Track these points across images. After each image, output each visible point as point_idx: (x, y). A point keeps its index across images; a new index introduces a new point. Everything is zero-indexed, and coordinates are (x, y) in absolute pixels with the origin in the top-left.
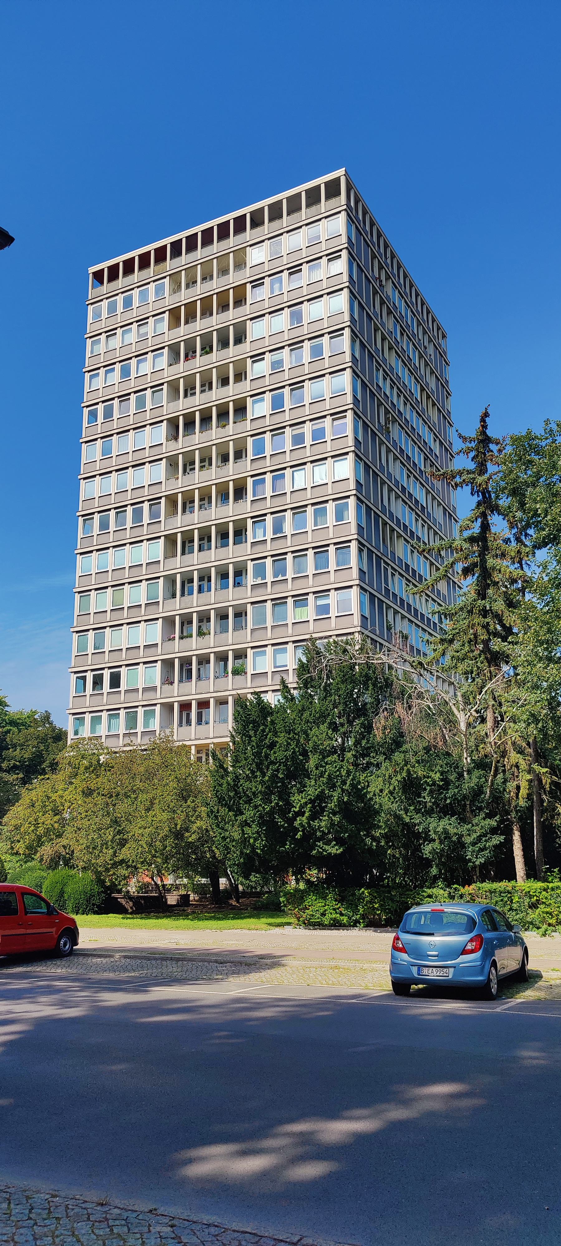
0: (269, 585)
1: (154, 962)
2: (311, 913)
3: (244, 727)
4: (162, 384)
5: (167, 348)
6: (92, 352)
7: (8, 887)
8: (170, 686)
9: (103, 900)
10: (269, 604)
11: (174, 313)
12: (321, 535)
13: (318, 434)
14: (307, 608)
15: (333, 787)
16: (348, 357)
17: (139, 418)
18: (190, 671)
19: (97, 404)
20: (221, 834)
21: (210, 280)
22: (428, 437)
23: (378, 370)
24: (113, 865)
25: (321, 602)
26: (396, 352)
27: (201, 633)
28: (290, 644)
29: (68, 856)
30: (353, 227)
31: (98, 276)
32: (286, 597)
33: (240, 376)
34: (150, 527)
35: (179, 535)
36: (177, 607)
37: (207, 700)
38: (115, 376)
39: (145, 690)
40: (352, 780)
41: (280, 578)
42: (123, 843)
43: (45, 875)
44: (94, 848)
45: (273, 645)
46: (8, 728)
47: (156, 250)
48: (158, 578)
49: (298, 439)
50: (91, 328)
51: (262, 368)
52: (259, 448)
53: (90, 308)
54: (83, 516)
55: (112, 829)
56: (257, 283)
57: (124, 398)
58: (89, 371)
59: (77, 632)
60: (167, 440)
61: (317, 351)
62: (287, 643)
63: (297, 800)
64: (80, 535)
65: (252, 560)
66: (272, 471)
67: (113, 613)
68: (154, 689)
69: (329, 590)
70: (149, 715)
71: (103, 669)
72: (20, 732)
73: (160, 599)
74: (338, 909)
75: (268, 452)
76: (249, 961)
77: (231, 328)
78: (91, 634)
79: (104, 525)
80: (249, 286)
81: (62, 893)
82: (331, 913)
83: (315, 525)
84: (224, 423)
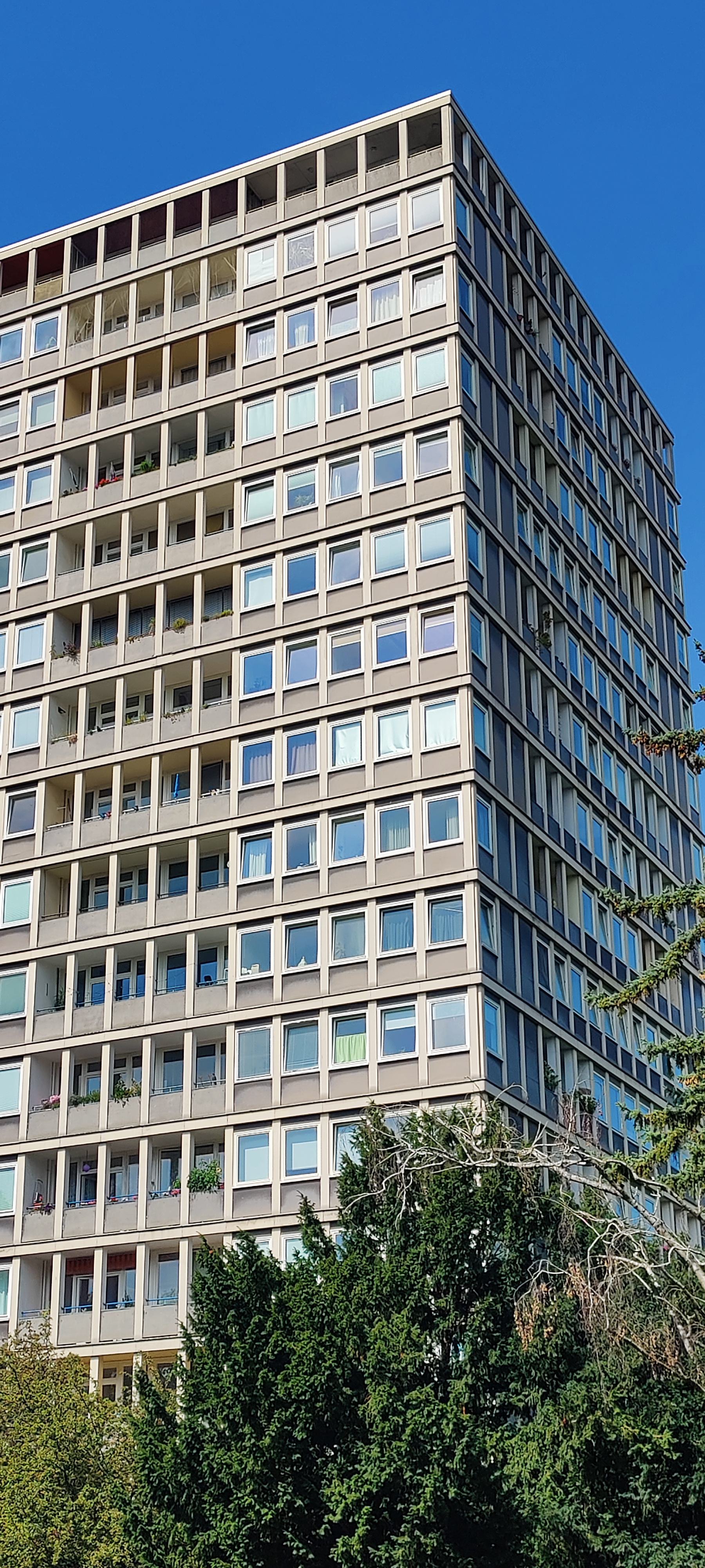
3: (216, 1318)
4: (47, 534)
8: (45, 1216)
13: (392, 648)
15: (421, 1462)
21: (157, 315)
22: (634, 657)
25: (395, 1023)
27: (119, 1093)
30: (469, 210)
40: (468, 1446)
41: (302, 967)
48: (25, 963)
49: (346, 658)
51: (270, 502)
52: (260, 675)
56: (260, 323)
60: (54, 657)
62: (316, 1117)
63: (339, 1494)
65: (240, 925)
69: (413, 996)
73: (29, 1012)
77: (201, 416)
80: (241, 329)
83: (384, 848)
84: (182, 620)
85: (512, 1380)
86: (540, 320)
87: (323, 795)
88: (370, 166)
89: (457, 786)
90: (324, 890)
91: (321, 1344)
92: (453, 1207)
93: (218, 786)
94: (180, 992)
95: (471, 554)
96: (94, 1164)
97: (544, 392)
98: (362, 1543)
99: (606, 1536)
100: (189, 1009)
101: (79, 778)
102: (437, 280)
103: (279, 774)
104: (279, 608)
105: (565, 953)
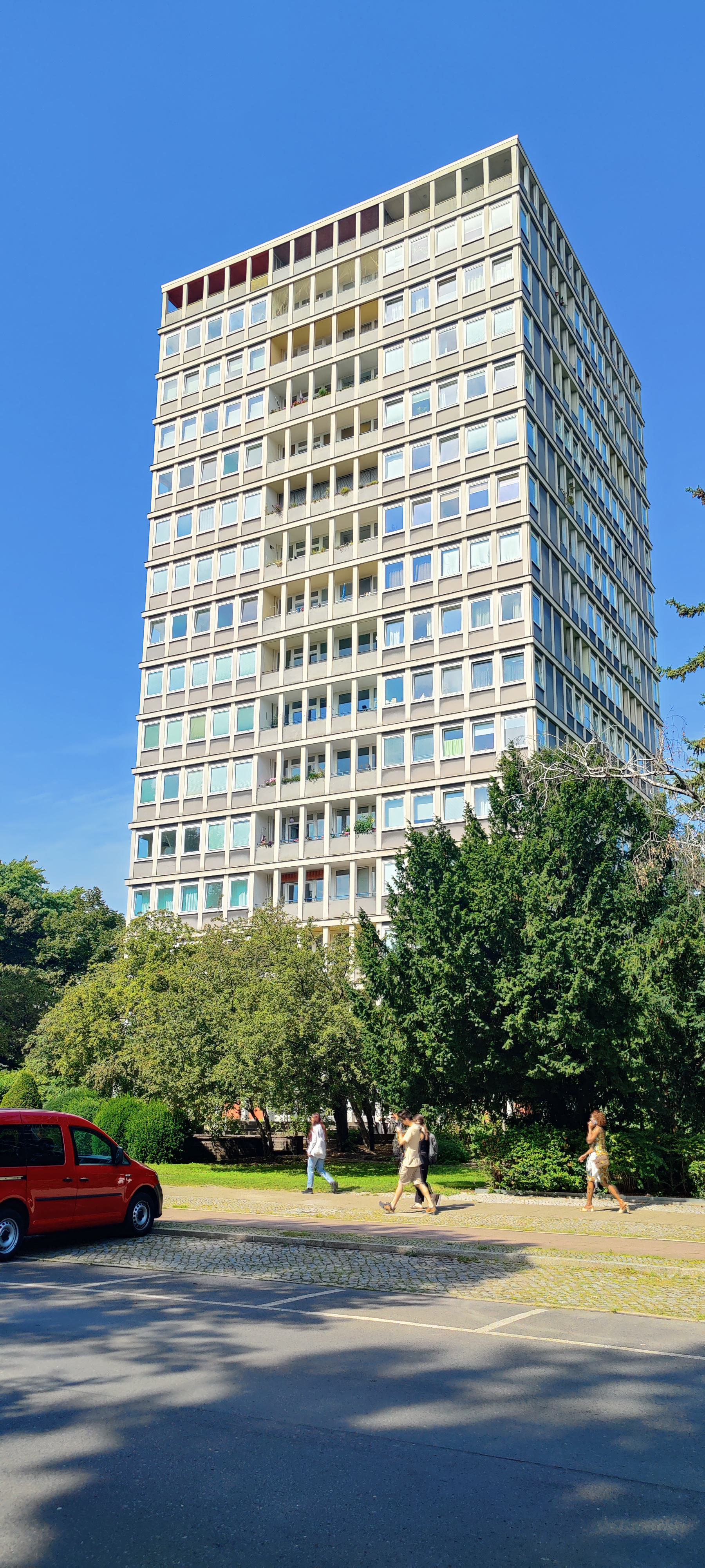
0: (408, 708)
1: (294, 1249)
2: (522, 1169)
3: (421, 872)
4: (261, 438)
6: (165, 398)
7: (46, 1116)
8: (268, 848)
9: (181, 1142)
10: (408, 735)
11: (278, 343)
12: (482, 639)
13: (479, 501)
14: (458, 739)
15: (568, 965)
16: (520, 394)
17: (228, 483)
18: (295, 830)
19: (172, 466)
20: (376, 1042)
21: (327, 296)
22: (620, 518)
23: (558, 418)
24: (200, 1089)
25: (481, 732)
26: (581, 397)
27: (311, 776)
28: (438, 790)
29: (129, 1078)
30: (528, 217)
31: (175, 297)
32: (432, 725)
33: (367, 426)
34: (242, 631)
35: (282, 642)
36: (278, 739)
37: (320, 867)
38: (197, 429)
39: (234, 853)
40: (604, 954)
41: (423, 698)
42: (214, 1060)
43: (97, 1104)
44: (172, 1064)
45: (413, 791)
46: (45, 909)
47: (254, 258)
48: (253, 700)
49: (450, 509)
50: (163, 366)
51: (401, 411)
52: (395, 521)
53: (161, 383)
54: (150, 617)
55: (199, 1036)
56: (393, 297)
57: (208, 457)
58: (161, 423)
59: (141, 774)
60: (267, 514)
61: (477, 388)
62: (432, 788)
63: (506, 988)
64: (147, 643)
65: (384, 674)
66: (412, 553)
67: (190, 748)
68: (246, 852)
69: (493, 715)
70: (238, 888)
71: (176, 824)
72: (60, 915)
73: (256, 729)
74: (566, 1163)
75: (408, 526)
76: (465, 1252)
77: (357, 359)
78: (160, 777)
79: (179, 630)
80: (382, 302)
81: (121, 1130)
82: (555, 1171)
83: (474, 626)
84: (346, 488)
85: (612, 919)
86: (568, 298)
87: (436, 593)
88: (464, 190)
89: (520, 585)
90: (436, 652)
91: (496, 889)
92: (572, 806)
93: (369, 590)
94: (348, 716)
96: (297, 818)
97: (570, 345)
98: (524, 1018)
99: (688, 1017)
100: (354, 725)
101: (284, 588)
102: (508, 263)
103: (408, 580)
104: (407, 478)
105: (581, 692)
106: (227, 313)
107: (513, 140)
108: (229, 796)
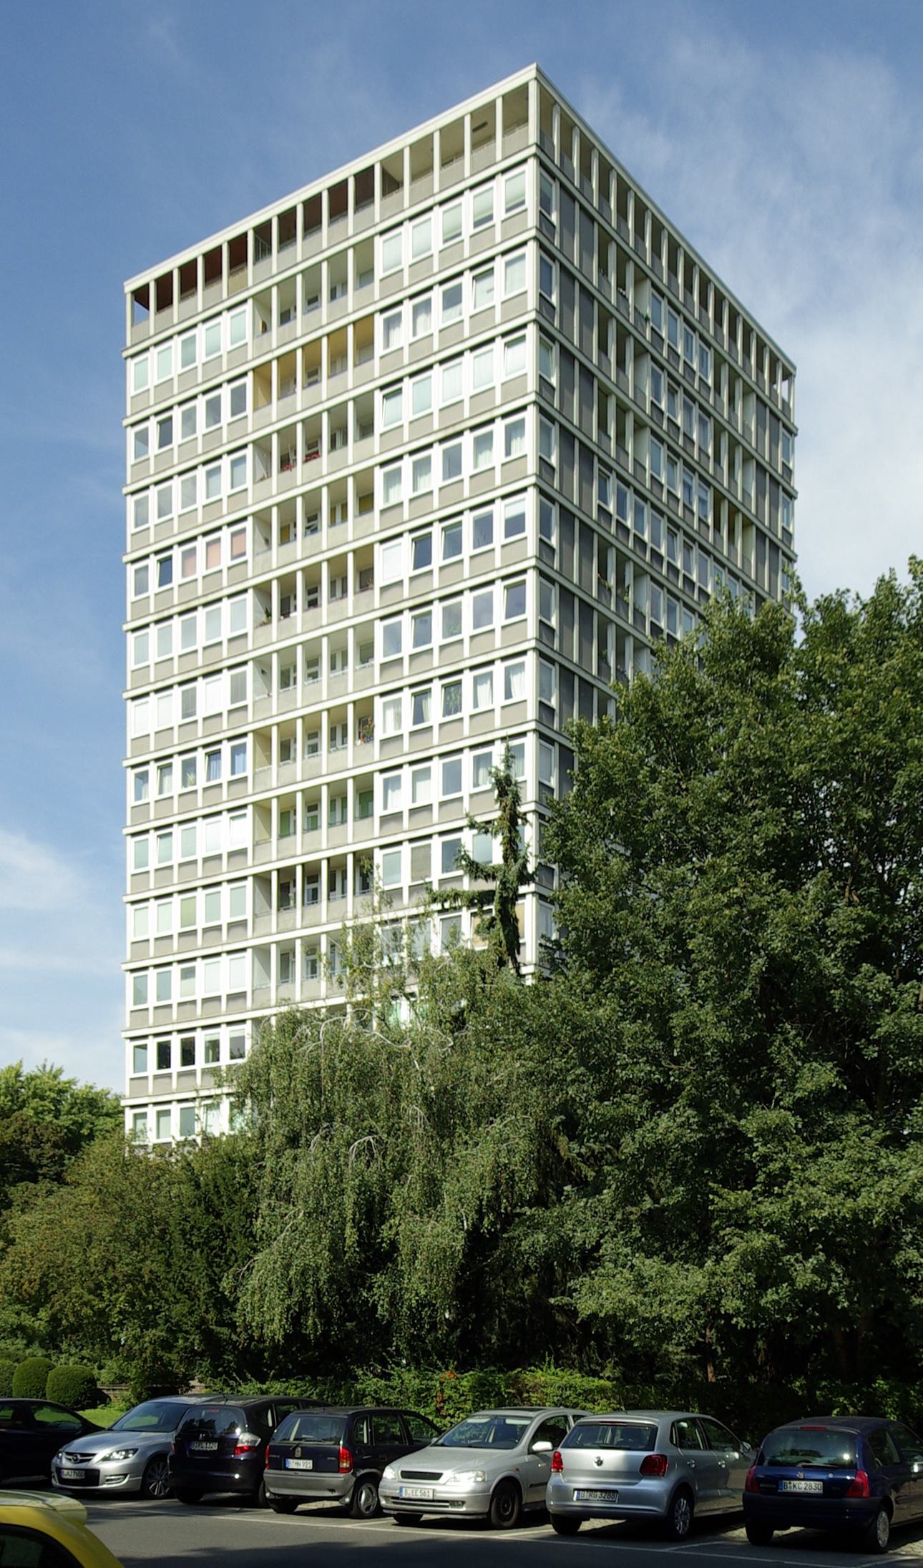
5: (250, 447)
31: (140, 296)
53: (131, 364)
80: (378, 395)
95: (544, 202)
106: (202, 328)
107: (527, 75)
108: (224, 999)
